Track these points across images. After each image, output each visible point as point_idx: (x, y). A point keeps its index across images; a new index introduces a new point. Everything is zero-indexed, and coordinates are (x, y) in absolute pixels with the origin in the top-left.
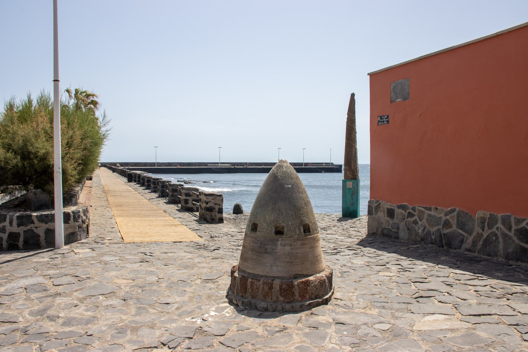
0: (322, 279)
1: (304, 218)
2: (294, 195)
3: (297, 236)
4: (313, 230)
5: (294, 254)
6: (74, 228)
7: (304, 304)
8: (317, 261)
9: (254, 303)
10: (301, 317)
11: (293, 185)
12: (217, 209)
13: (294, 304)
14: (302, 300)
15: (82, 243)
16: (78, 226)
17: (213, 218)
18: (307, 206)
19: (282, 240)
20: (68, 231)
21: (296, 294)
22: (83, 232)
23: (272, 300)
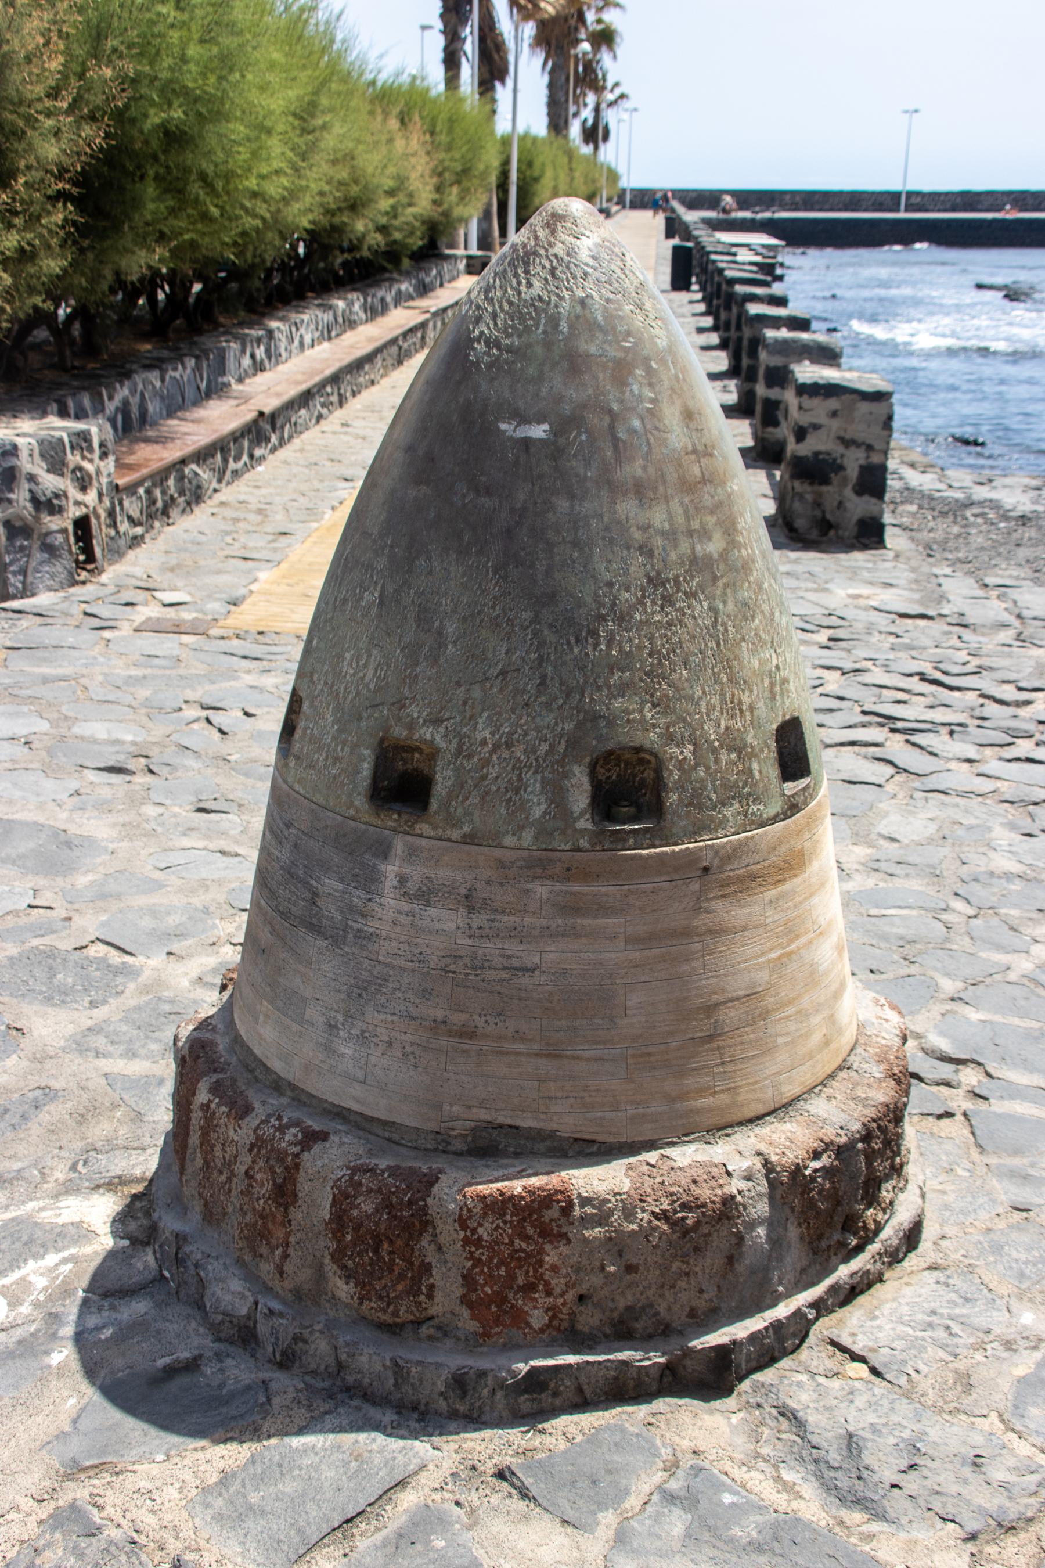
0: (705, 1193)
1: (617, 704)
2: (563, 504)
3: (528, 837)
4: (696, 801)
5: (490, 974)
7: (482, 1374)
8: (711, 1038)
9: (197, 1266)
10: (423, 1467)
11: (563, 426)
12: (853, 472)
13: (409, 1353)
14: (486, 1335)
15: (19, 612)
17: (828, 516)
18: (668, 600)
19: (412, 853)
21: (437, 1276)
22: (38, 556)
23: (286, 1284)
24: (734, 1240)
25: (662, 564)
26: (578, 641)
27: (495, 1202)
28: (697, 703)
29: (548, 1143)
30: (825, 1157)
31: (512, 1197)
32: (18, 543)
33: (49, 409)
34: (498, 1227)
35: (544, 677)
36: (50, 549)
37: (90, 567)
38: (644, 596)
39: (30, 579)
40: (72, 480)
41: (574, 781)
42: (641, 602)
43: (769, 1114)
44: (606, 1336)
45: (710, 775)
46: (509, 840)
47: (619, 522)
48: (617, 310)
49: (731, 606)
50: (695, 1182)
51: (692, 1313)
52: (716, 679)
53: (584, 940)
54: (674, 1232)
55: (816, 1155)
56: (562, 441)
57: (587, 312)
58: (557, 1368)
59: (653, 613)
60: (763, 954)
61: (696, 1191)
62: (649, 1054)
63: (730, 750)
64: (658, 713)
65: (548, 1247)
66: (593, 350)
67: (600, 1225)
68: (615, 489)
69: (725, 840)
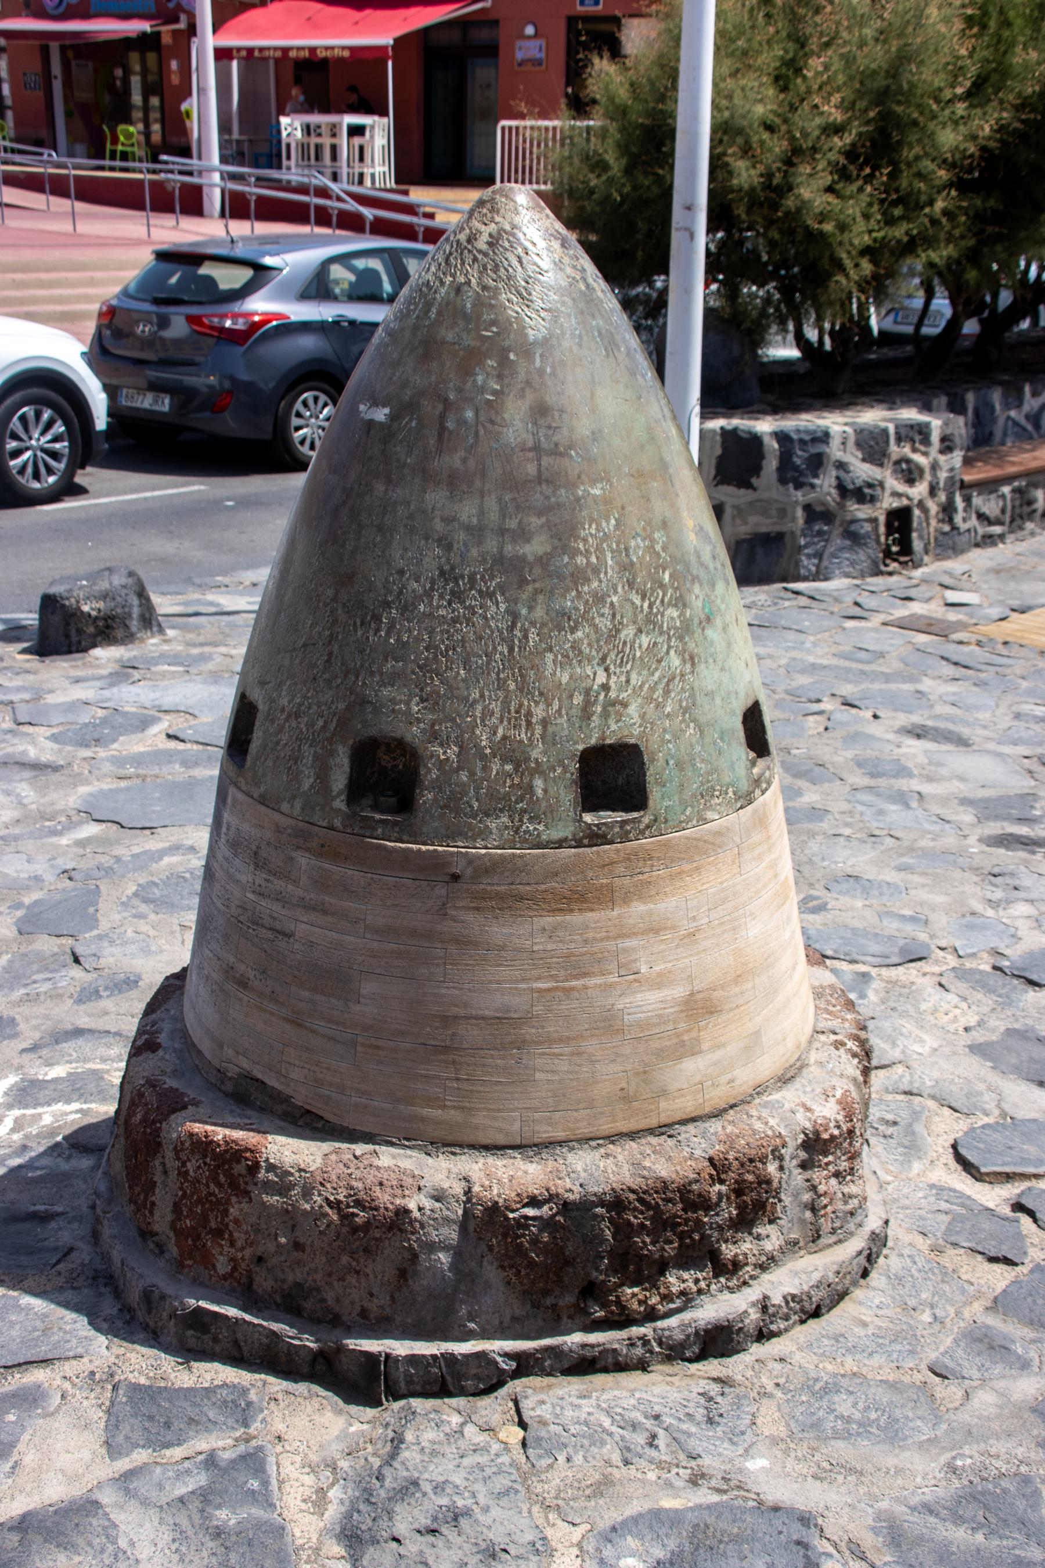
0: (383, 1198)
2: (380, 487)
3: (298, 804)
4: (453, 803)
6: (783, 513)
8: (446, 1050)
16: (808, 508)
18: (458, 596)
20: (746, 523)
24: (407, 1255)
25: (458, 560)
26: (362, 624)
27: (199, 1142)
28: (471, 706)
29: (284, 1107)
30: (546, 1208)
31: (212, 1141)
32: (817, 528)
33: (935, 402)
34: (199, 1167)
35: (330, 654)
36: (855, 538)
37: (902, 559)
38: (432, 589)
39: (825, 563)
40: (894, 472)
41: (338, 760)
42: (428, 594)
43: (513, 1147)
44: (277, 1305)
45: (475, 781)
46: (285, 807)
47: (424, 512)
48: (490, 298)
49: (539, 613)
50: (381, 1184)
51: (364, 1313)
52: (501, 684)
53: (329, 918)
54: (342, 1225)
55: (534, 1202)
56: (395, 425)
57: (459, 299)
58: (216, 1314)
59: (439, 607)
60: (524, 980)
61: (377, 1192)
62: (378, 1047)
63: (504, 760)
64: (425, 708)
65: (234, 1199)
66: (450, 337)
67: (280, 1195)
68: (427, 477)
69: (483, 851)
